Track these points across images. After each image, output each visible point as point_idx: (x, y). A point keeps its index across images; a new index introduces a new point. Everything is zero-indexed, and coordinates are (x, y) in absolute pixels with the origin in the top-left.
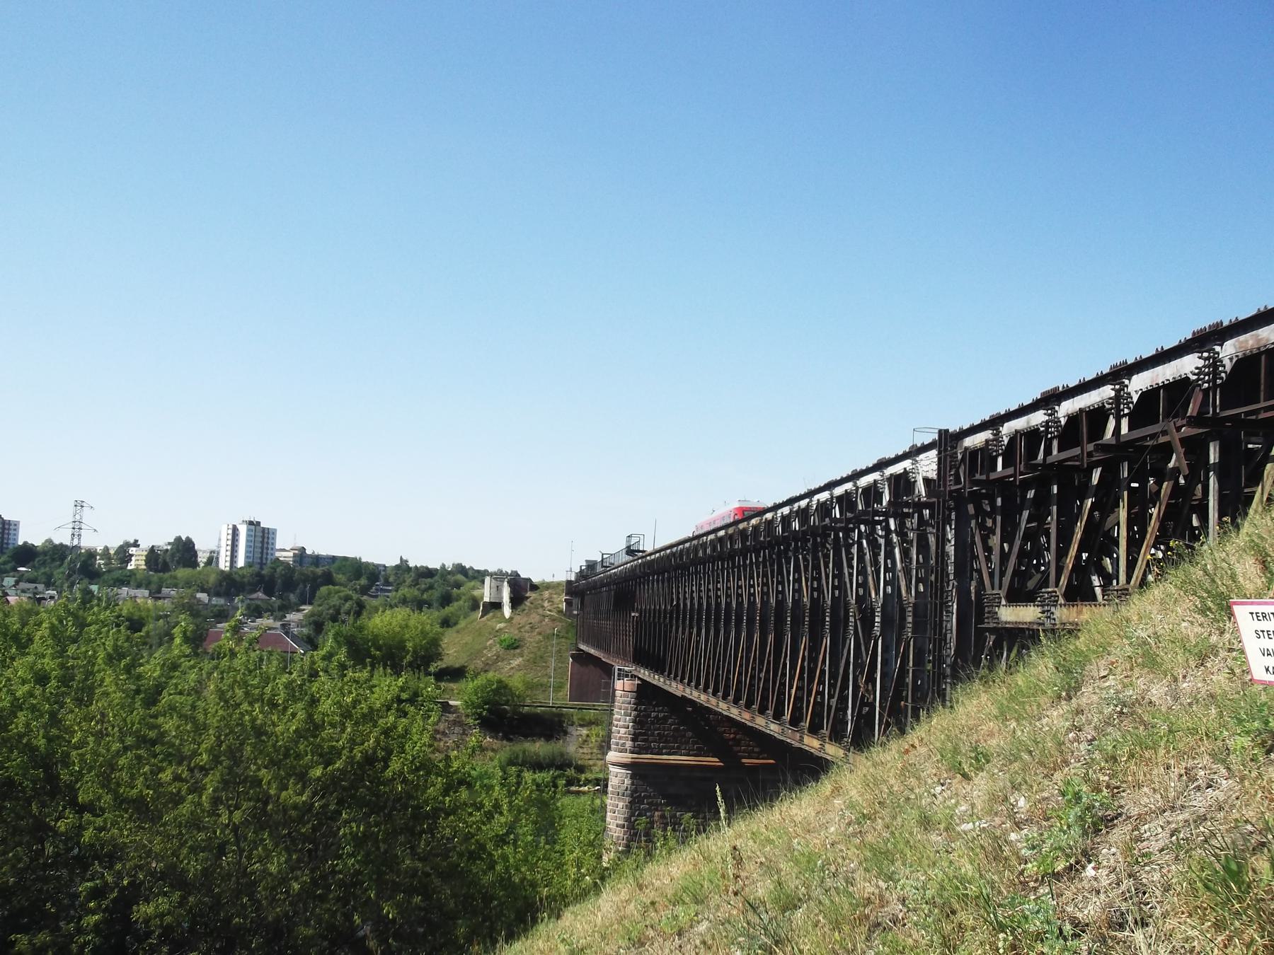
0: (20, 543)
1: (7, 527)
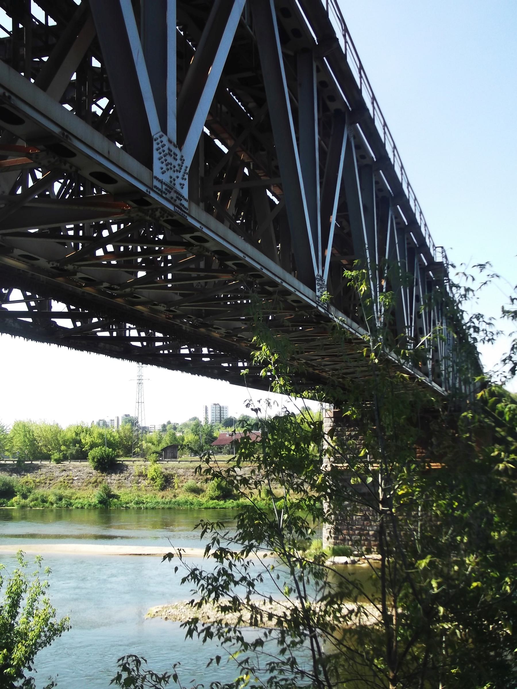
0: (229, 417)
1: (222, 409)
